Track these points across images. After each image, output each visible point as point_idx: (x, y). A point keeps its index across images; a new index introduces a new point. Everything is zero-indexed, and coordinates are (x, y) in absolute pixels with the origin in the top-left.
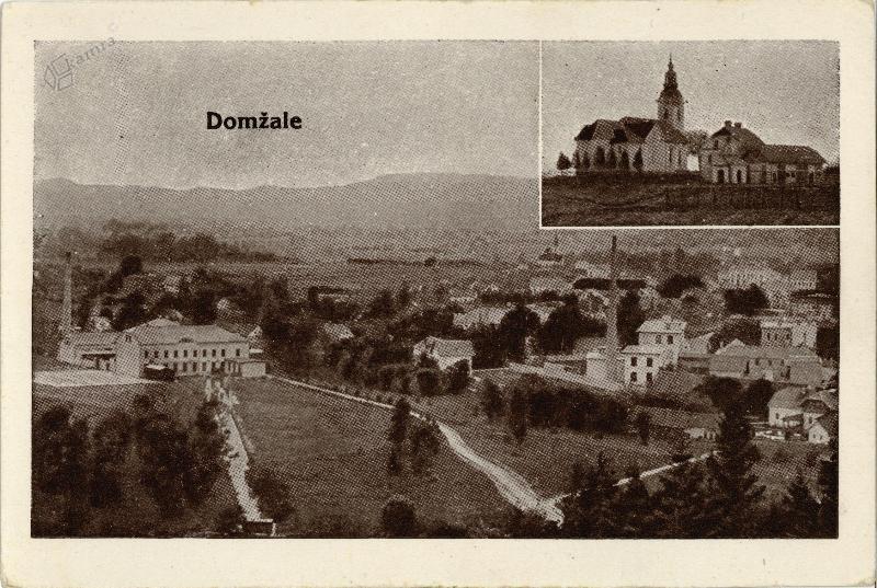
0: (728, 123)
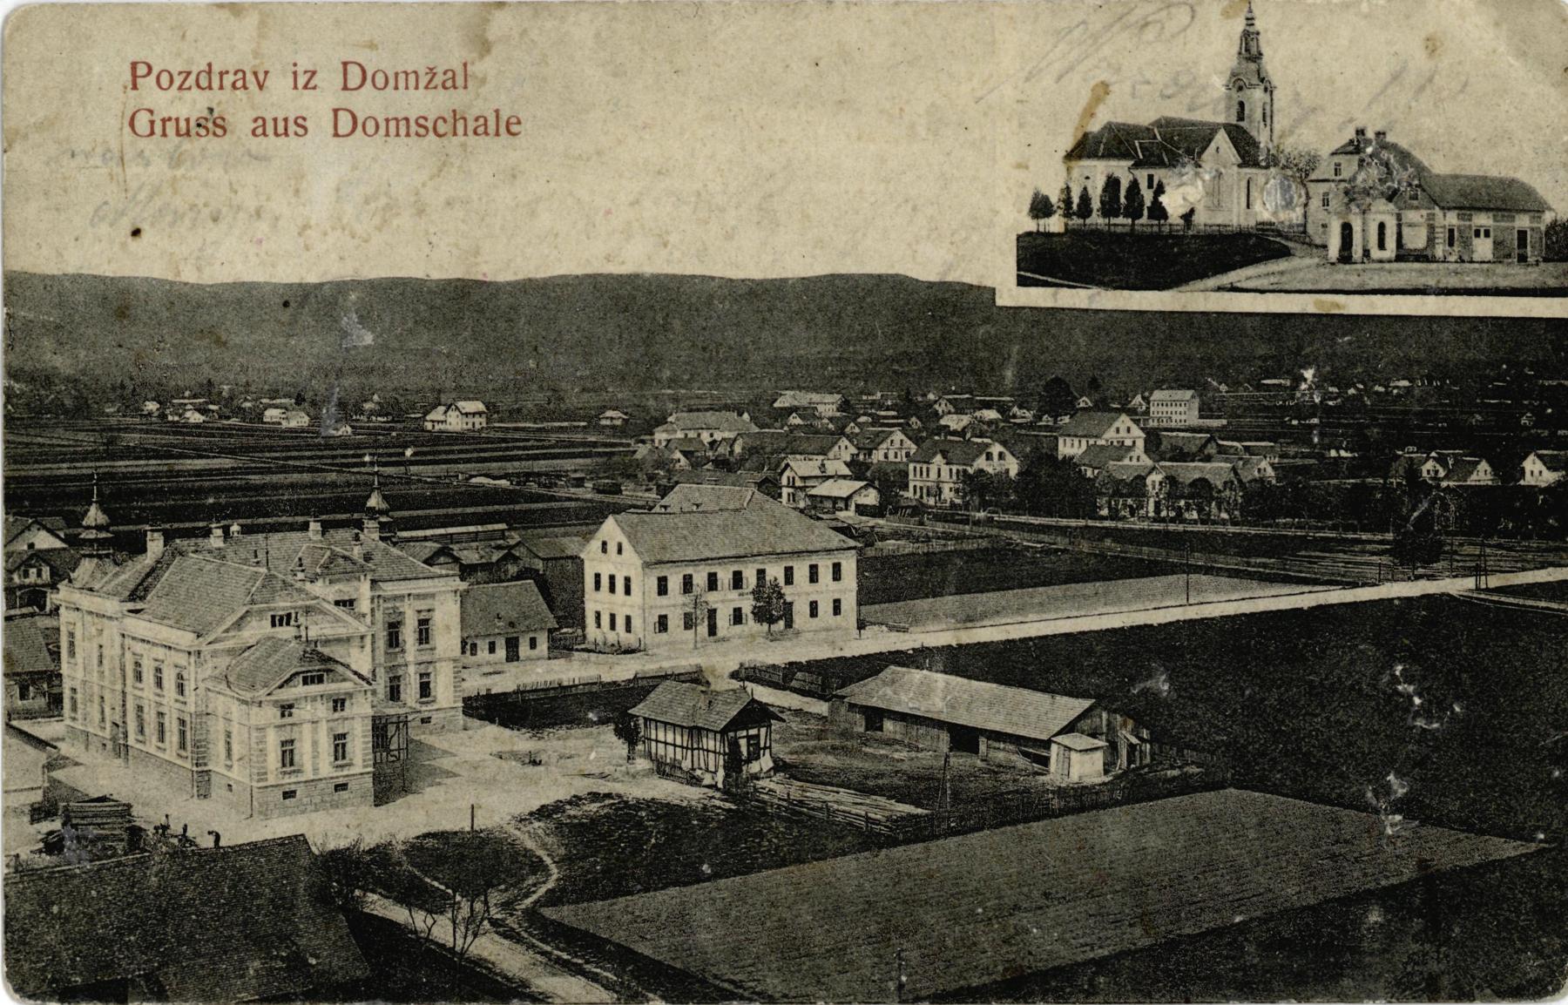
0: (1360, 132)
